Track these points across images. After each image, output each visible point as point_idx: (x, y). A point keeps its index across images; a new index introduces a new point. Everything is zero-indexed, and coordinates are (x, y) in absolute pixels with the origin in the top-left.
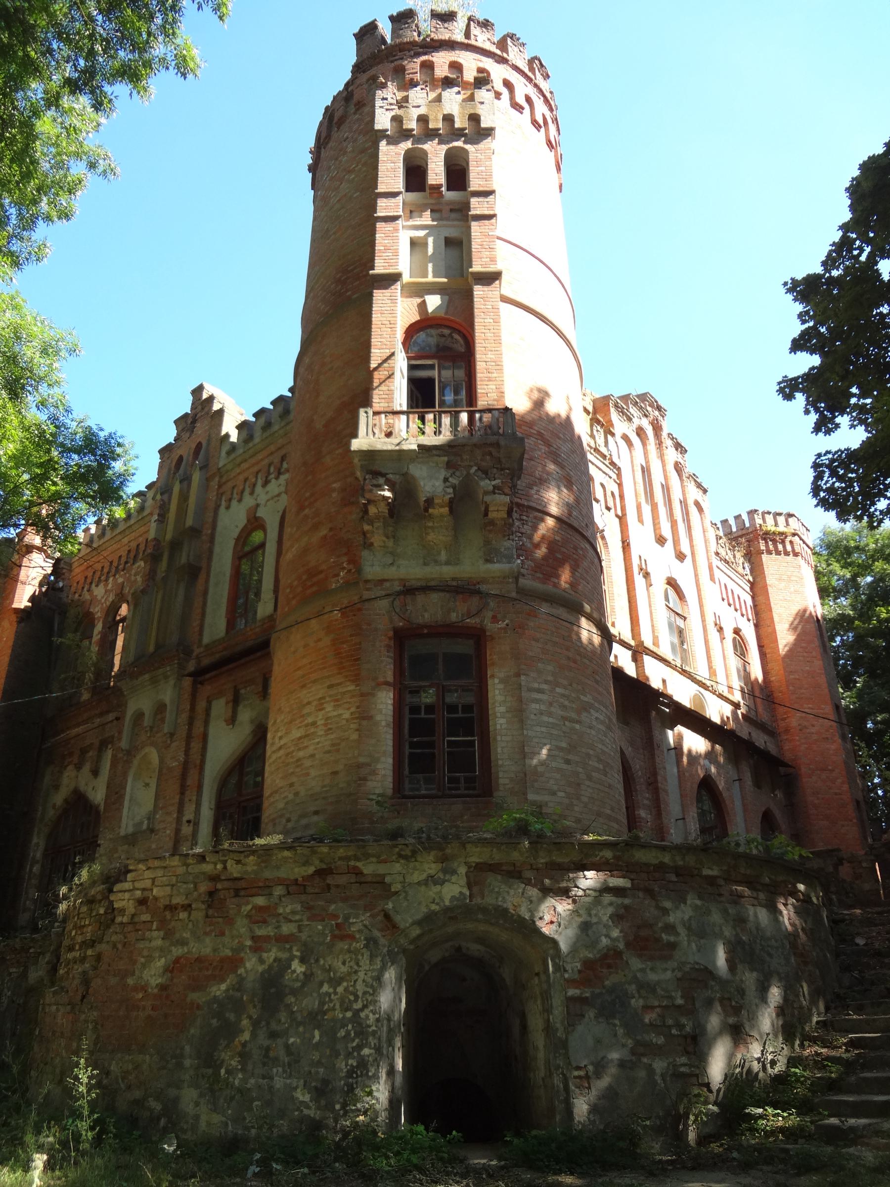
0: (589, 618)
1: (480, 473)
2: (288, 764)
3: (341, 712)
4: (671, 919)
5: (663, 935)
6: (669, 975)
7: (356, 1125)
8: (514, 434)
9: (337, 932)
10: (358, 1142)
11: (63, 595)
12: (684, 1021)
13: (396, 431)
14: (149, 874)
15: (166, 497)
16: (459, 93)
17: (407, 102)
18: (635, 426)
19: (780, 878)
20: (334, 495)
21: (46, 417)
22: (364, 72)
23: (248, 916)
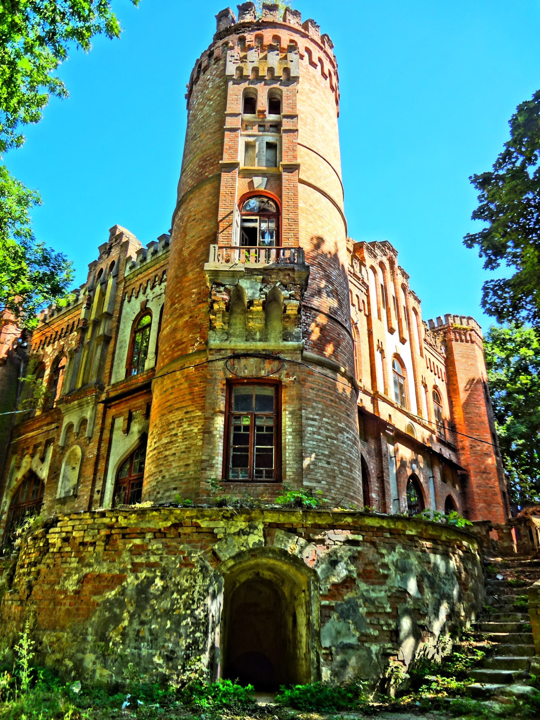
0: (344, 375)
1: (282, 286)
2: (159, 459)
3: (192, 428)
4: (386, 560)
5: (381, 570)
6: (383, 594)
7: (190, 679)
8: (304, 263)
9: (183, 561)
10: (191, 689)
12: (390, 622)
13: (232, 259)
14: (70, 523)
15: (91, 293)
16: (278, 54)
17: (246, 59)
18: (378, 261)
19: (453, 538)
20: (193, 296)
21: (19, 243)
22: (221, 39)
23: (130, 550)
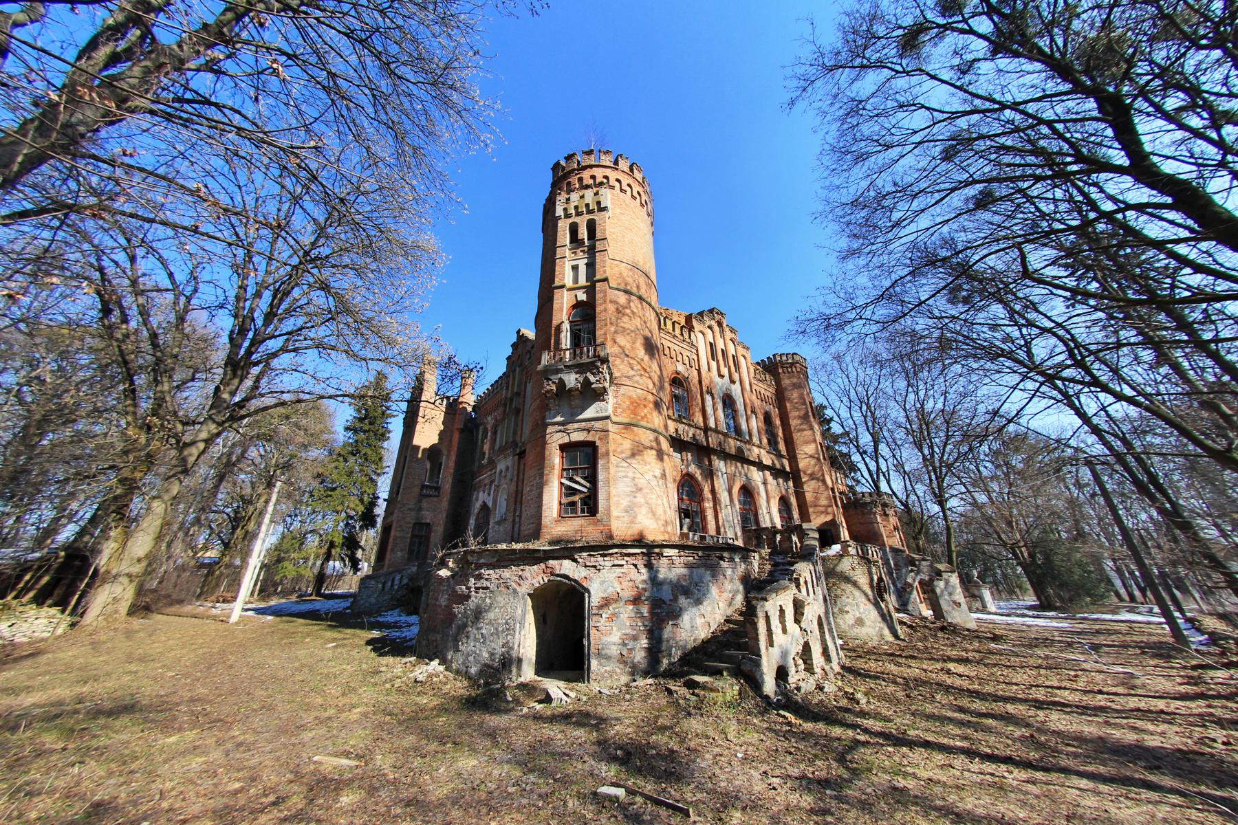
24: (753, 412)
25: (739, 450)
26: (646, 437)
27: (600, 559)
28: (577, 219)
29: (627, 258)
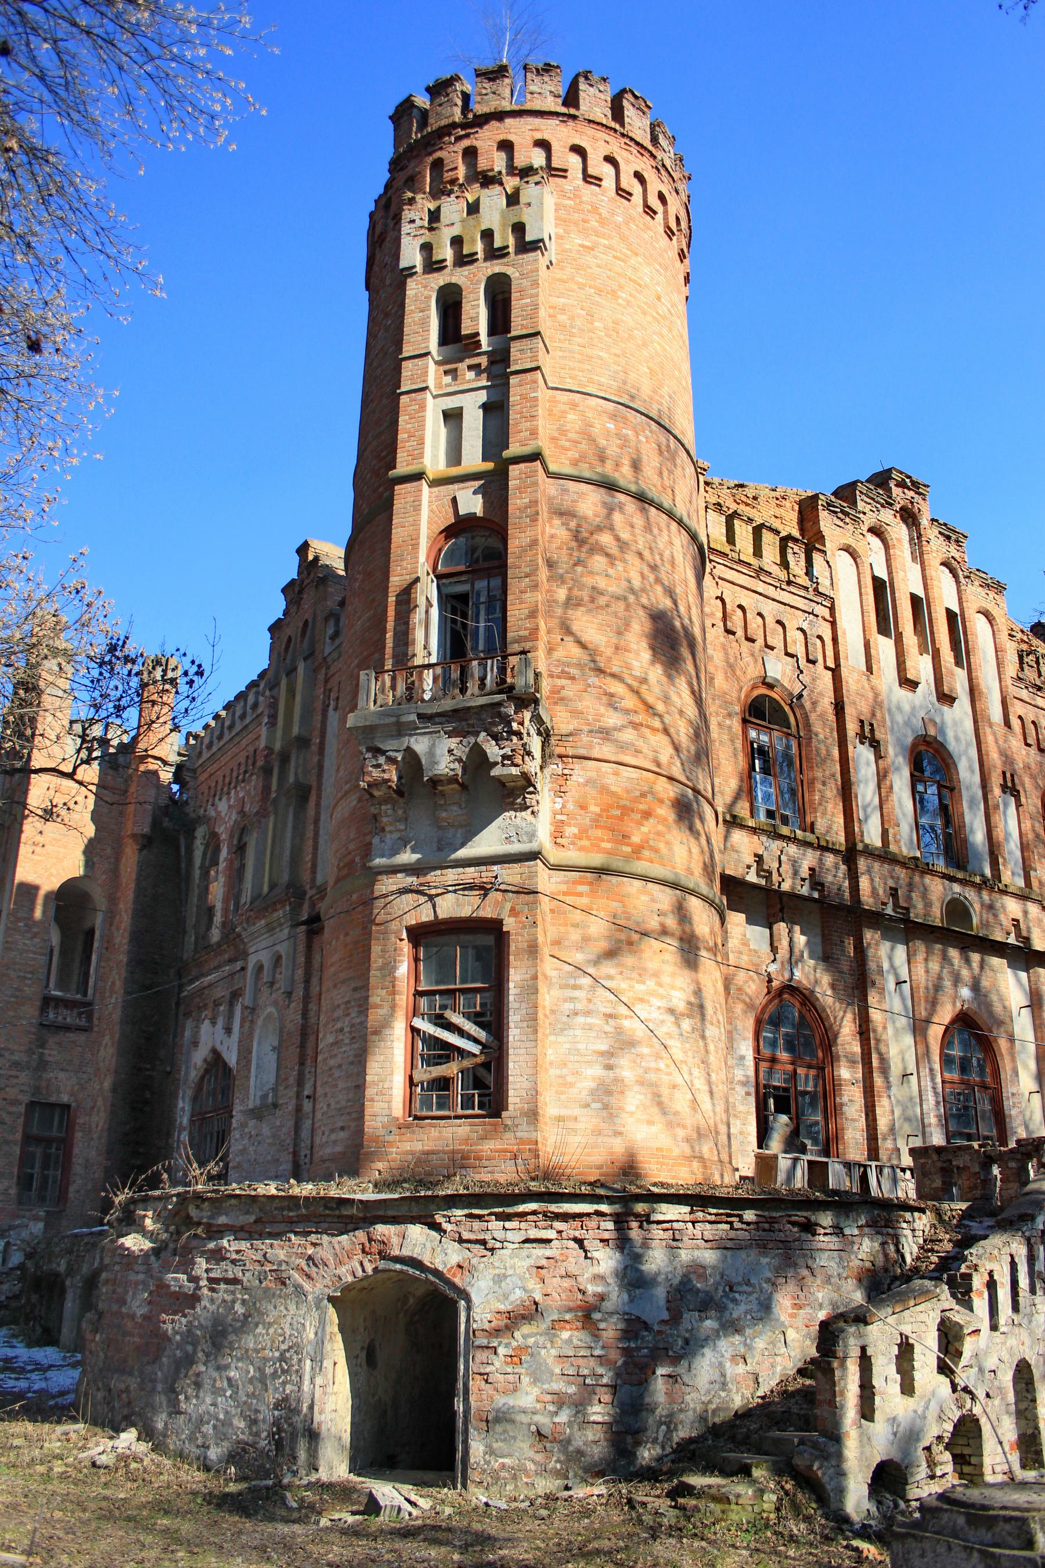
11: (189, 810)
24: (1011, 789)
25: (957, 909)
26: (650, 904)
27: (495, 1225)
28: (459, 276)
29: (605, 381)
